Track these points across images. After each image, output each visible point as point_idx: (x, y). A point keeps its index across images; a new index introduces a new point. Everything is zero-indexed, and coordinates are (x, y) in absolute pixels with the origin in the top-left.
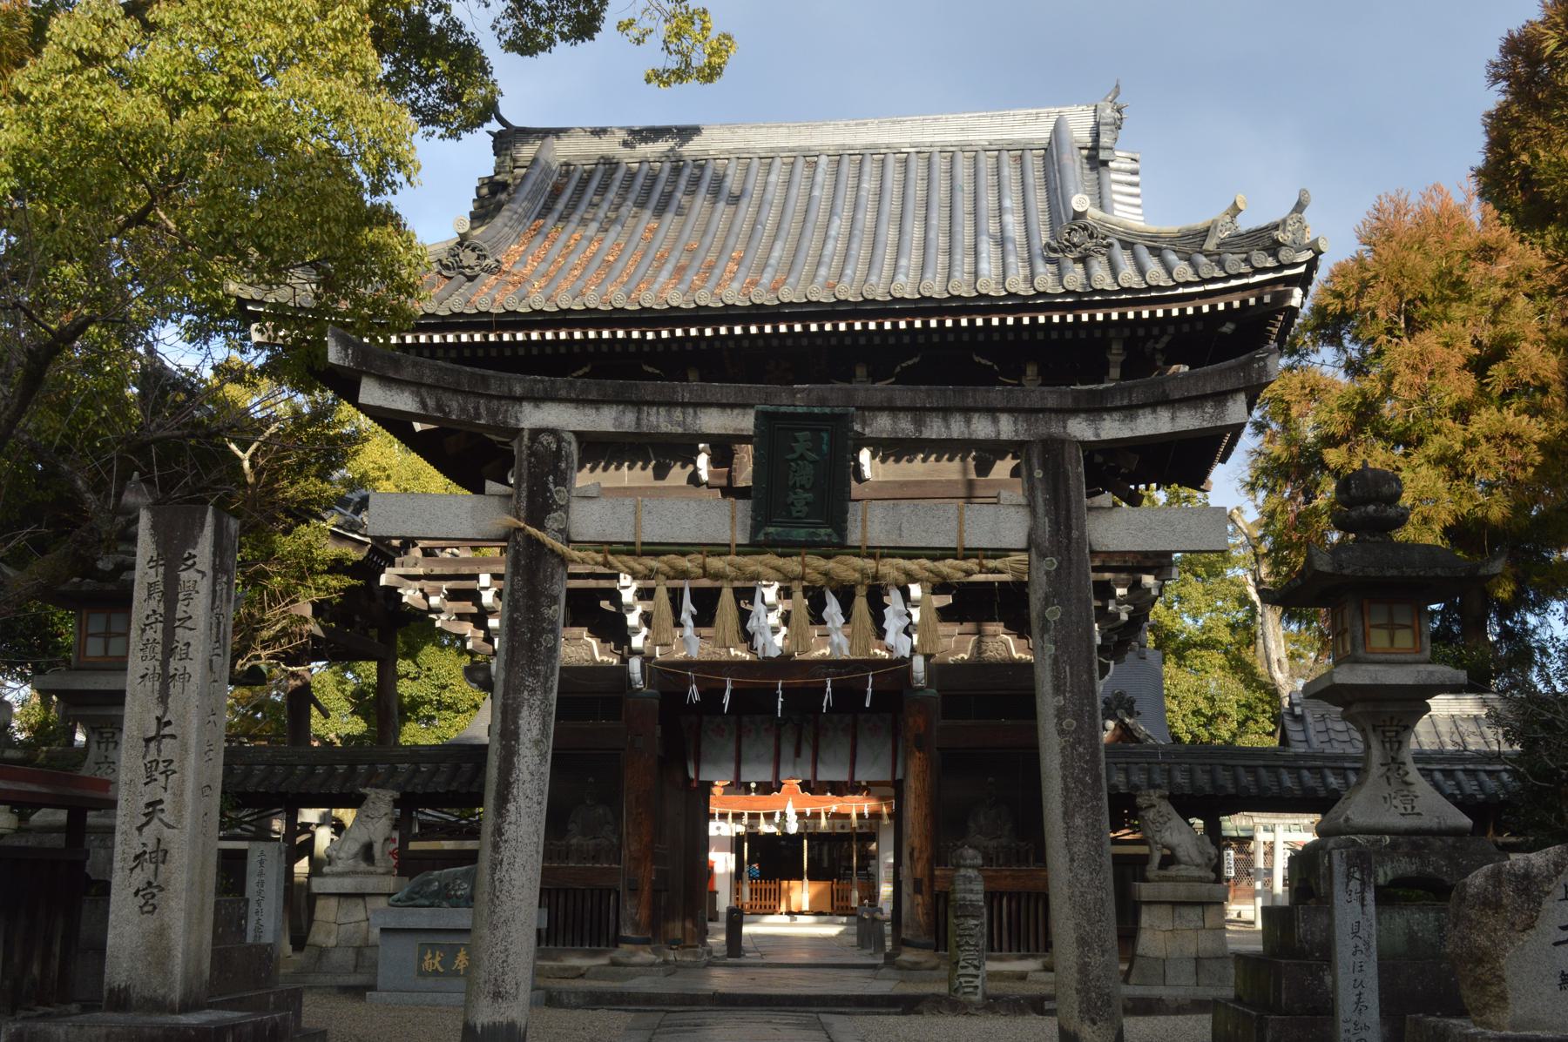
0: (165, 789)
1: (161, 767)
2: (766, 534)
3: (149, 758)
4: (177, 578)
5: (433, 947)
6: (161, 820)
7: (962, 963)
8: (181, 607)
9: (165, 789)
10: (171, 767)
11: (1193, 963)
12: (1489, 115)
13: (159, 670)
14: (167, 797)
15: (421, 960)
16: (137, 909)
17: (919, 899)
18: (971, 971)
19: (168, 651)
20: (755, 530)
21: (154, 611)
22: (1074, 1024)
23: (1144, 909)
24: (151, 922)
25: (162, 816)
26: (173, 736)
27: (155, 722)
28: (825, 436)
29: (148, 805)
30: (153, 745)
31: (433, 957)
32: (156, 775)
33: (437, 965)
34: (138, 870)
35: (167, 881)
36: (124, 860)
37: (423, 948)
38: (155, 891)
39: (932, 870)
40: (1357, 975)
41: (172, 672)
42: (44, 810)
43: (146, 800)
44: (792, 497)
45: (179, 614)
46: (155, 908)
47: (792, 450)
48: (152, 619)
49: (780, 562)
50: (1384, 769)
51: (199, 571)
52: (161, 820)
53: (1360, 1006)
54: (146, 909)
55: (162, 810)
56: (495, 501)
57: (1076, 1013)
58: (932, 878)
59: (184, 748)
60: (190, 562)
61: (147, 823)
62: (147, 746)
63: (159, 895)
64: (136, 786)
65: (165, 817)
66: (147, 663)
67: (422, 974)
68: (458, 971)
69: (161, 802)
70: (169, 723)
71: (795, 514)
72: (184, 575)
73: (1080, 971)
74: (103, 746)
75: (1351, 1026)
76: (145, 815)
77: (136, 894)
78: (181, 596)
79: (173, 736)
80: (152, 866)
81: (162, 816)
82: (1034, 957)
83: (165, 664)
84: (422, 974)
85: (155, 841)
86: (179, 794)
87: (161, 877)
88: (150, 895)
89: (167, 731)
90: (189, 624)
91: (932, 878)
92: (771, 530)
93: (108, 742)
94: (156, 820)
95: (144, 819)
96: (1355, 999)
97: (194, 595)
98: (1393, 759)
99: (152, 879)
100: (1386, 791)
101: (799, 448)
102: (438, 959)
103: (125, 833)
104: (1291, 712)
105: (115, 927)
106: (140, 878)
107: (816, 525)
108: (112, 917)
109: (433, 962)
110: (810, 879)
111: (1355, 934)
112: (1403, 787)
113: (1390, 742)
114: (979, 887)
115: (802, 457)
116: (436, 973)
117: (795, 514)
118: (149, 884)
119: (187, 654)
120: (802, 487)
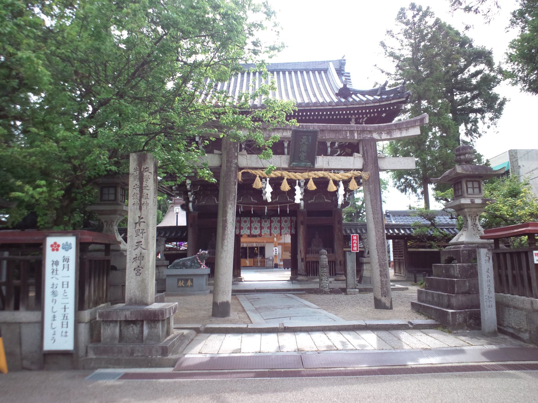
0: (142, 238)
1: (141, 231)
2: (293, 165)
3: (137, 229)
4: (143, 174)
5: (181, 280)
6: (141, 247)
7: (323, 280)
8: (144, 183)
9: (142, 238)
10: (144, 231)
11: (160, 268)
12: (490, 53)
13: (139, 202)
14: (143, 240)
15: (178, 283)
16: (135, 274)
17: (303, 263)
18: (326, 282)
19: (141, 197)
20: (290, 163)
21: (136, 185)
22: (379, 297)
23: (364, 264)
24: (139, 278)
25: (142, 246)
26: (144, 222)
27: (138, 218)
28: (310, 137)
29: (137, 243)
30: (138, 225)
31: (181, 282)
32: (139, 234)
33: (183, 284)
34: (135, 262)
35: (144, 266)
36: (130, 259)
37: (178, 280)
38: (140, 269)
39: (306, 256)
40: (488, 283)
41: (142, 203)
42: (92, 245)
43: (136, 241)
44: (301, 154)
45: (144, 185)
46: (140, 274)
47: (301, 141)
48: (136, 187)
49: (294, 174)
50: (472, 226)
51: (150, 172)
52: (141, 247)
53: (489, 292)
54: (138, 274)
55: (142, 244)
56: (217, 156)
57: (380, 294)
58: (306, 258)
59: (148, 225)
60: (147, 170)
61: (137, 248)
62: (136, 225)
63: (142, 270)
64: (133, 237)
65: (143, 246)
66: (134, 200)
67: (179, 287)
68: (188, 286)
69: (141, 242)
70: (143, 218)
71: (301, 159)
72: (145, 174)
73: (381, 283)
74: (108, 226)
75: (487, 297)
76: (136, 246)
77: (134, 269)
78: (144, 180)
79: (144, 222)
80: (139, 261)
81: (142, 246)
82: (333, 277)
83: (140, 200)
84: (179, 287)
85: (140, 254)
86: (147, 239)
87: (142, 265)
88: (139, 270)
89: (142, 220)
90: (147, 188)
91: (306, 258)
92: (294, 163)
93: (109, 225)
94: (139, 248)
95: (136, 247)
96: (488, 290)
97: (148, 179)
98: (474, 224)
99: (139, 265)
100: (474, 232)
101: (303, 141)
102: (183, 282)
103: (130, 251)
104: (386, 215)
105: (128, 280)
106: (135, 265)
107: (307, 162)
108: (127, 277)
109: (181, 283)
110: (249, 258)
111: (488, 272)
112: (478, 231)
113: (473, 219)
114: (327, 260)
115: (304, 143)
116: (182, 286)
117: (301, 159)
118: (139, 266)
119: (147, 197)
120: (304, 152)
